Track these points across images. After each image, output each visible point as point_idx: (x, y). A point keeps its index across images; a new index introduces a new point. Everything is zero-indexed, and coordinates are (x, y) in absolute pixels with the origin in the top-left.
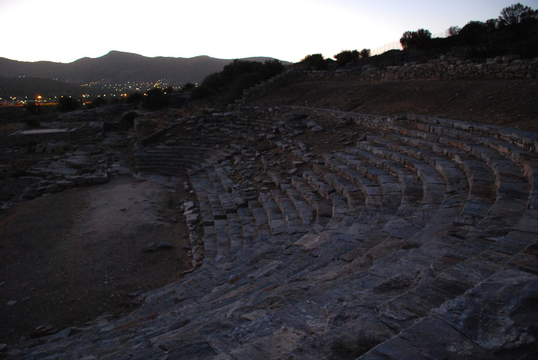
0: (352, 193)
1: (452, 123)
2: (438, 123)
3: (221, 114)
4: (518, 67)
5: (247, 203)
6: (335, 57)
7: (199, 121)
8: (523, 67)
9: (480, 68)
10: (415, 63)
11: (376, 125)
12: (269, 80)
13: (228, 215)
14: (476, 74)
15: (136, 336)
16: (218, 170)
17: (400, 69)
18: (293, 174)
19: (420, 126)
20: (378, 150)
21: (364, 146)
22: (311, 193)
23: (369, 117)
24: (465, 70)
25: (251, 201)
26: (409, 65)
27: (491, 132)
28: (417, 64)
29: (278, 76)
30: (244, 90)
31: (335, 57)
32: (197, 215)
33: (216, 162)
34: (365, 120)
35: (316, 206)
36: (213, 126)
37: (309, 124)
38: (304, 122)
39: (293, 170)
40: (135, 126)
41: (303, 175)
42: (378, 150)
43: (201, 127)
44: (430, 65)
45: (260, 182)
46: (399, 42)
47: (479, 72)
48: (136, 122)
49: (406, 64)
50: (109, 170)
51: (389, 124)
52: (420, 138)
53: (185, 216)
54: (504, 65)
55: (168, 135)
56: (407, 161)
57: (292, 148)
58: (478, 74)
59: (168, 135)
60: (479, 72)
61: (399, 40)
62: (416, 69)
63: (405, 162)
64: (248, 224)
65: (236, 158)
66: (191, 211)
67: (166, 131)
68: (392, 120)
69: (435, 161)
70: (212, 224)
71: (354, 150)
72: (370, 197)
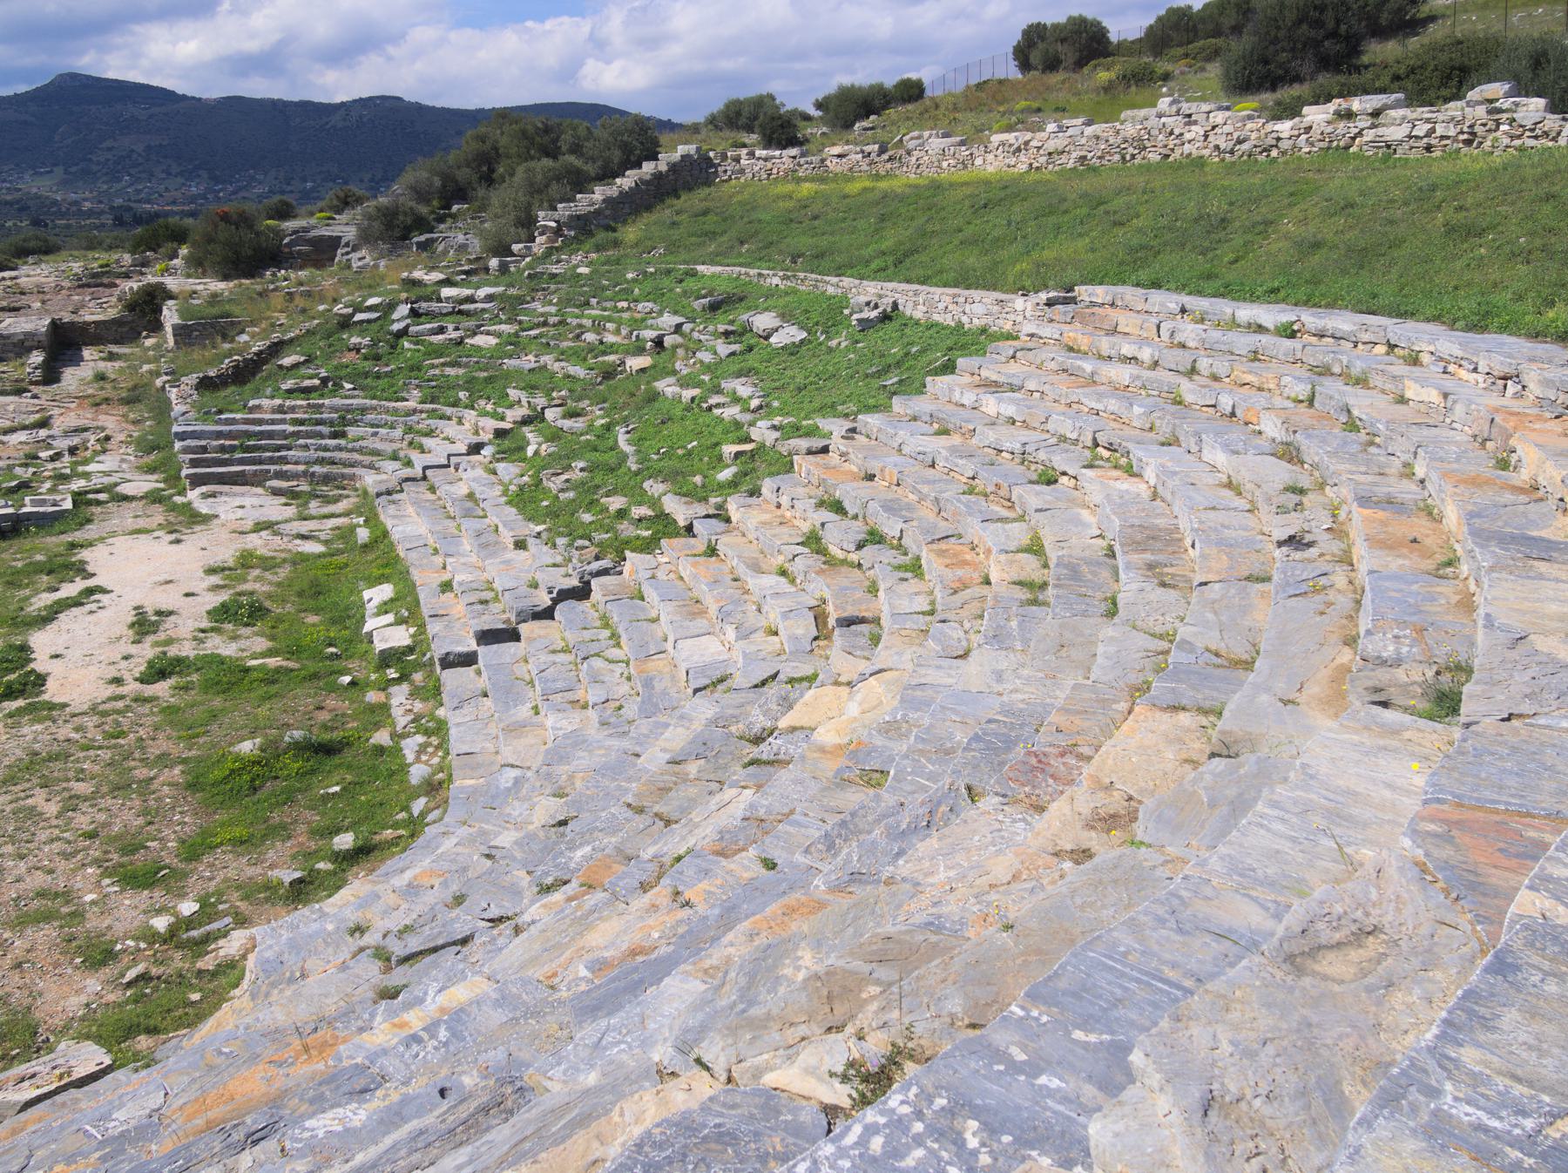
0: (934, 546)
1: (1229, 311)
2: (1183, 311)
3: (467, 292)
4: (1404, 130)
5: (588, 583)
6: (819, 105)
7: (395, 316)
8: (1421, 130)
9: (1285, 135)
10: (1080, 121)
11: (976, 321)
12: (618, 181)
13: (524, 629)
14: (1274, 153)
15: (726, 972)
16: (472, 476)
17: (1034, 143)
18: (733, 484)
19: (1126, 321)
20: (1000, 401)
21: (951, 390)
22: (800, 549)
23: (954, 296)
24: (1240, 142)
25: (603, 579)
26: (1061, 129)
27: (1366, 337)
28: (1089, 123)
29: (648, 168)
30: (541, 214)
31: (819, 105)
32: (412, 630)
33: (464, 449)
34: (941, 306)
35: (820, 588)
36: (442, 330)
37: (763, 321)
38: (745, 317)
39: (725, 475)
40: (169, 329)
41: (764, 491)
42: (1000, 401)
43: (403, 333)
44: (1130, 130)
45: (622, 514)
46: (1011, 56)
47: (1284, 145)
48: (170, 316)
49: (1051, 127)
50: (78, 485)
51: (1020, 319)
52: (1133, 359)
53: (370, 634)
54: (1361, 125)
55: (287, 361)
56: (1101, 438)
57: (714, 400)
58: (1284, 153)
59: (287, 361)
60: (1284, 145)
61: (1011, 50)
62: (1083, 141)
63: (1095, 439)
64: (597, 655)
65: (530, 436)
66: (390, 618)
67: (277, 349)
68: (1029, 306)
69: (1198, 435)
70: (468, 660)
71: (921, 404)
72: (1003, 557)
